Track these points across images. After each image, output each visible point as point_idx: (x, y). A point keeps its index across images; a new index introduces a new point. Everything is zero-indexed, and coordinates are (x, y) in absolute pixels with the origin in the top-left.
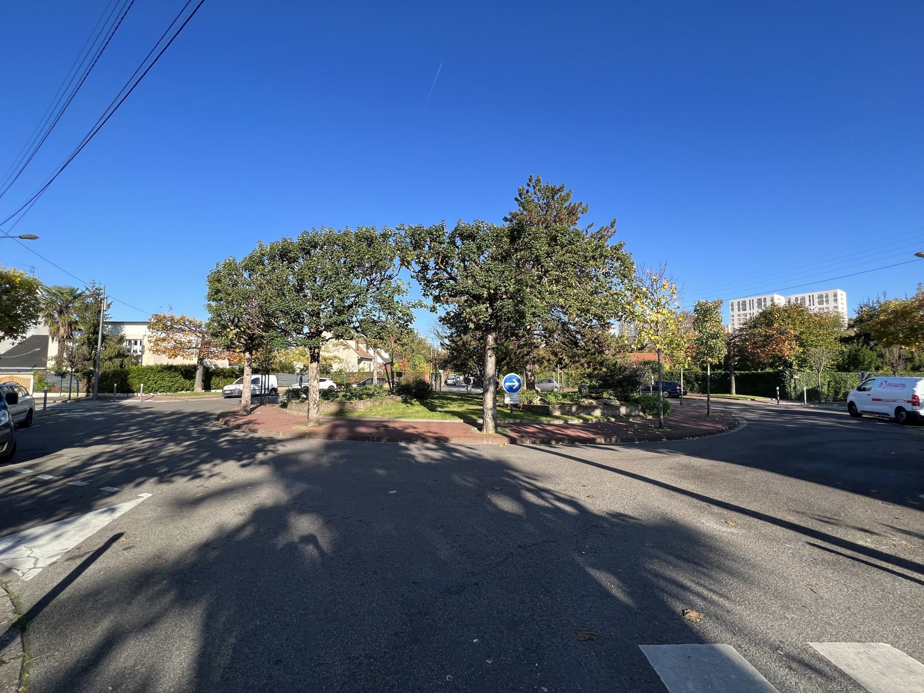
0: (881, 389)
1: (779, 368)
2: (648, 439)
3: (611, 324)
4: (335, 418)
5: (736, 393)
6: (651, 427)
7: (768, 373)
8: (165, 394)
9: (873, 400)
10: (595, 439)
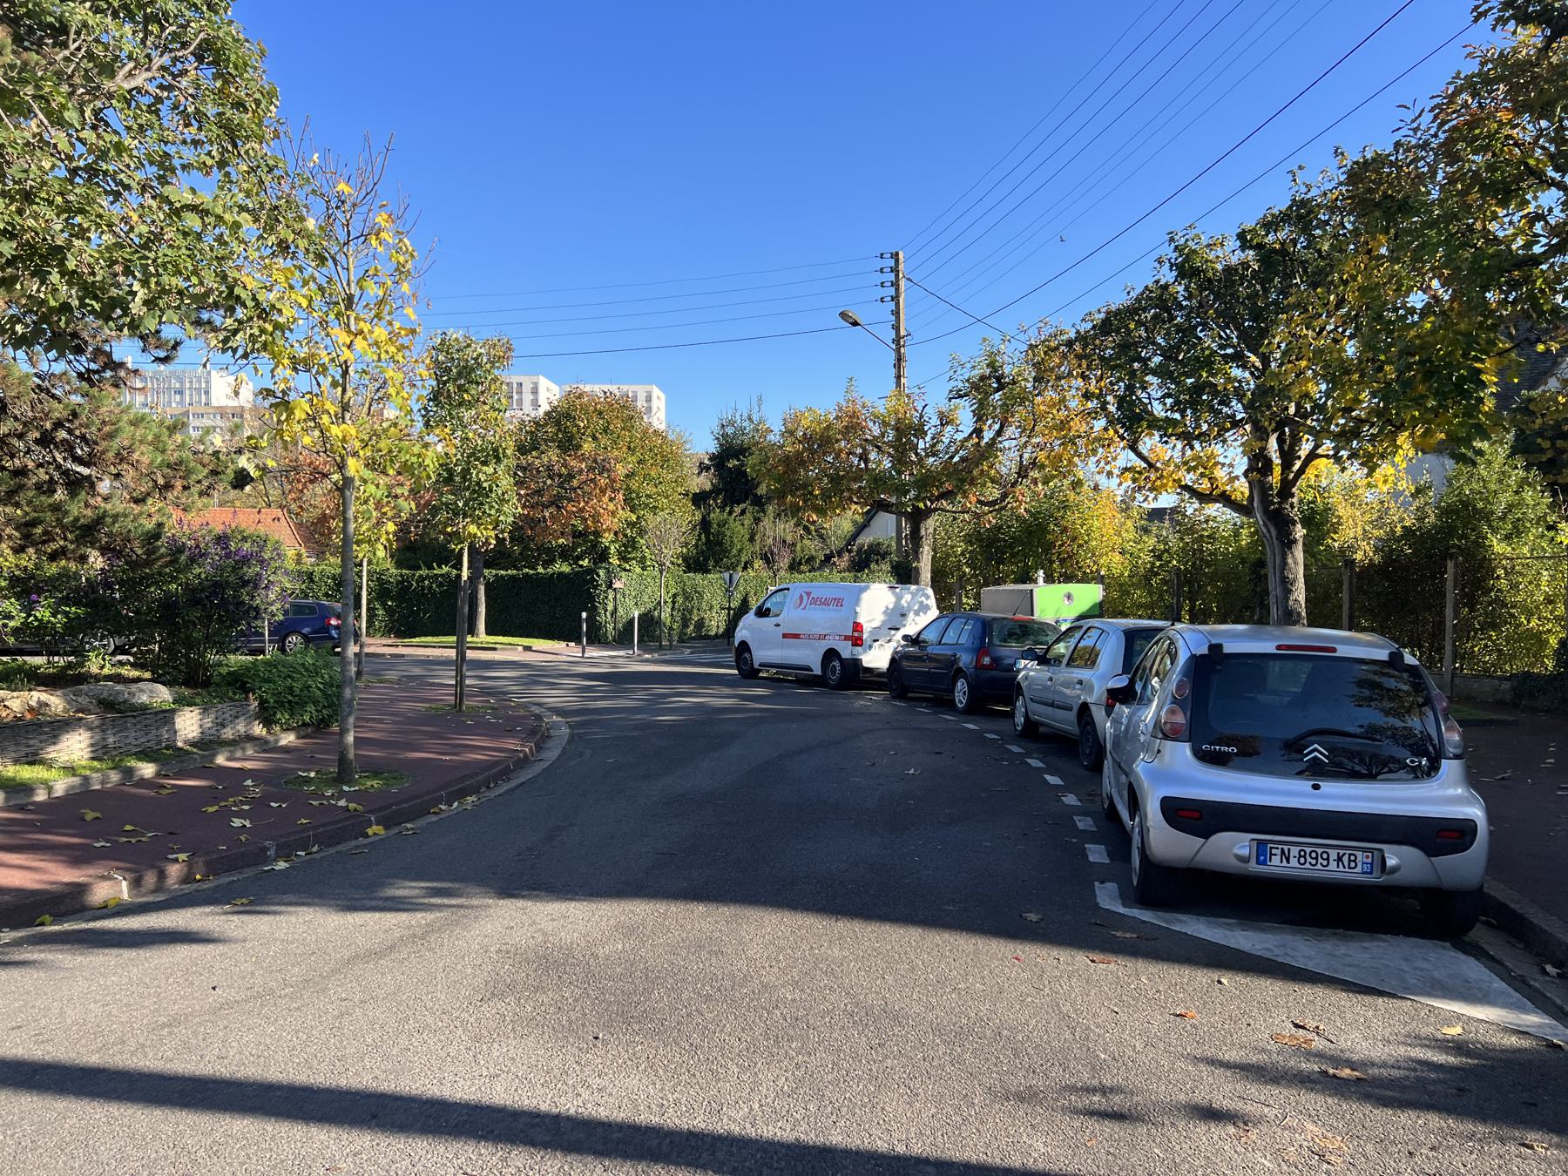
0: (799, 613)
1: (581, 563)
2: (318, 840)
3: (129, 371)
5: (489, 633)
6: (308, 781)
7: (561, 574)
9: (785, 636)
10: (80, 889)
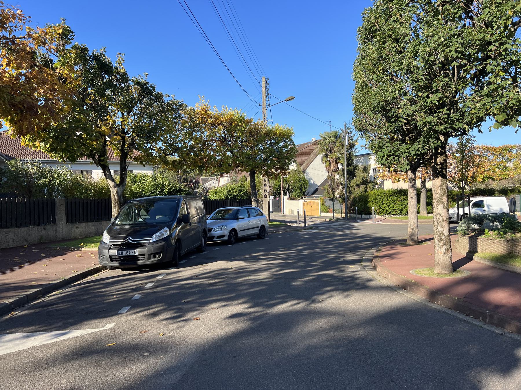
4: (492, 264)
8: (398, 216)
